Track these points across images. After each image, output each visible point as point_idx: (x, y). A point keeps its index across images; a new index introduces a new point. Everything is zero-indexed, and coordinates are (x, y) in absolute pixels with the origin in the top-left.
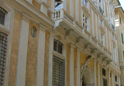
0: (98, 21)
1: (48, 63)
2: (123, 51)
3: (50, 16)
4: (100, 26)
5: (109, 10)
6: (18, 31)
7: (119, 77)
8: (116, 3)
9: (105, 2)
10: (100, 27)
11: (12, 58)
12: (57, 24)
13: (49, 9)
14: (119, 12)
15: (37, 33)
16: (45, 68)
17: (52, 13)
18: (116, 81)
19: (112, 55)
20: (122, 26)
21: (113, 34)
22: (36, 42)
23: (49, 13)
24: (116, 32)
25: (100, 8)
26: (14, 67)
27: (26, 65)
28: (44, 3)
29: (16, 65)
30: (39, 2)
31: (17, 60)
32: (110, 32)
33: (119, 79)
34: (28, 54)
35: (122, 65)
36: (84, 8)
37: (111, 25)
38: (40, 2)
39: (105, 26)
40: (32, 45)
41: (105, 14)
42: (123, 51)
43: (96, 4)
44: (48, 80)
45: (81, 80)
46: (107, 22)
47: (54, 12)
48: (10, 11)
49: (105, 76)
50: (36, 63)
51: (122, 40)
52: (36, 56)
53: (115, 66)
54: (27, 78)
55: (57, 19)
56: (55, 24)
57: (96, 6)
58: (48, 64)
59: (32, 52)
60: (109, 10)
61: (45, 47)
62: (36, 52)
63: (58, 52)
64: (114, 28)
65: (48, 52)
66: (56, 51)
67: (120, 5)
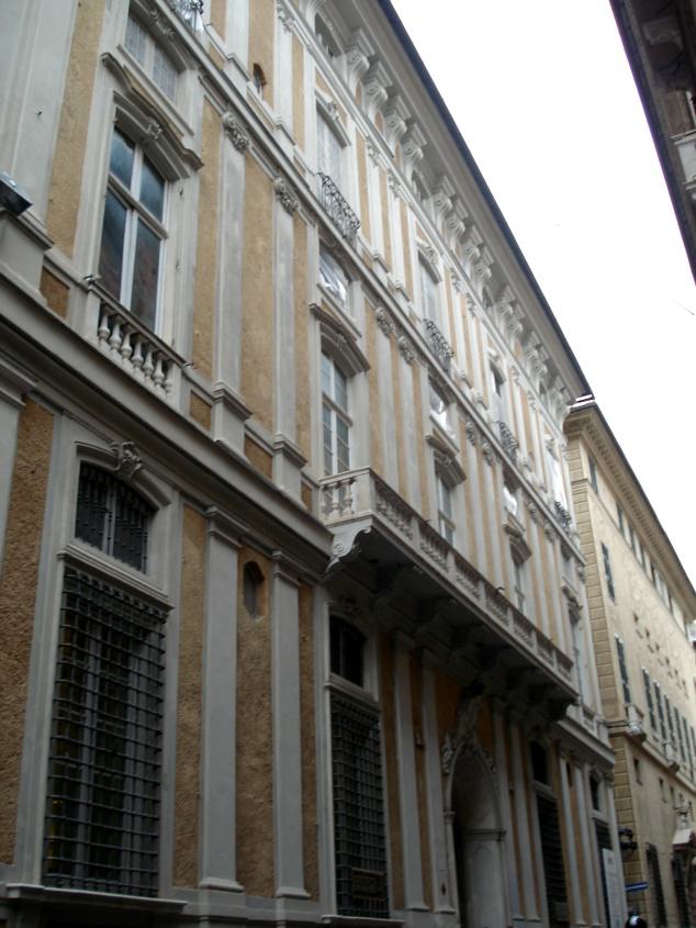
0: (497, 496)
1: (313, 738)
2: (110, 9)
3: (311, 499)
4: (435, 432)
5: (542, 428)
6: (196, 593)
7: (558, 756)
8: (568, 390)
9: (522, 391)
10: (432, 442)
11: (183, 727)
12: (343, 545)
13: (55, 253)
14: (584, 433)
15: (267, 593)
16: (304, 762)
17: (317, 487)
18: (596, 807)
19: (574, 669)
20: (600, 500)
21: (567, 552)
22: (266, 638)
23: (308, 487)
24: (578, 541)
25: (502, 426)
26: (189, 770)
27: (234, 756)
28: (286, 445)
29: (198, 761)
30: (264, 438)
31: (200, 735)
32: (554, 545)
33: (607, 798)
34: (239, 703)
35: (616, 715)
36: (438, 445)
37: (553, 508)
38: (271, 443)
39: (399, 353)
40: (252, 658)
41: (522, 456)
42: (110, 9)
43: (386, 271)
44: (317, 826)
45: (445, 810)
46: (536, 493)
47: (324, 483)
48: (166, 503)
49: (139, 568)
50: (269, 745)
51: (606, 577)
52: (269, 707)
53: (586, 723)
54: (239, 818)
55: (345, 518)
56: (336, 542)
57: (290, 155)
58: (314, 744)
59: (253, 693)
60: (538, 429)
61: (301, 657)
62: (267, 690)
63: (117, 555)
64: (514, 451)
65: (312, 682)
66: (100, 548)
67: (593, 398)
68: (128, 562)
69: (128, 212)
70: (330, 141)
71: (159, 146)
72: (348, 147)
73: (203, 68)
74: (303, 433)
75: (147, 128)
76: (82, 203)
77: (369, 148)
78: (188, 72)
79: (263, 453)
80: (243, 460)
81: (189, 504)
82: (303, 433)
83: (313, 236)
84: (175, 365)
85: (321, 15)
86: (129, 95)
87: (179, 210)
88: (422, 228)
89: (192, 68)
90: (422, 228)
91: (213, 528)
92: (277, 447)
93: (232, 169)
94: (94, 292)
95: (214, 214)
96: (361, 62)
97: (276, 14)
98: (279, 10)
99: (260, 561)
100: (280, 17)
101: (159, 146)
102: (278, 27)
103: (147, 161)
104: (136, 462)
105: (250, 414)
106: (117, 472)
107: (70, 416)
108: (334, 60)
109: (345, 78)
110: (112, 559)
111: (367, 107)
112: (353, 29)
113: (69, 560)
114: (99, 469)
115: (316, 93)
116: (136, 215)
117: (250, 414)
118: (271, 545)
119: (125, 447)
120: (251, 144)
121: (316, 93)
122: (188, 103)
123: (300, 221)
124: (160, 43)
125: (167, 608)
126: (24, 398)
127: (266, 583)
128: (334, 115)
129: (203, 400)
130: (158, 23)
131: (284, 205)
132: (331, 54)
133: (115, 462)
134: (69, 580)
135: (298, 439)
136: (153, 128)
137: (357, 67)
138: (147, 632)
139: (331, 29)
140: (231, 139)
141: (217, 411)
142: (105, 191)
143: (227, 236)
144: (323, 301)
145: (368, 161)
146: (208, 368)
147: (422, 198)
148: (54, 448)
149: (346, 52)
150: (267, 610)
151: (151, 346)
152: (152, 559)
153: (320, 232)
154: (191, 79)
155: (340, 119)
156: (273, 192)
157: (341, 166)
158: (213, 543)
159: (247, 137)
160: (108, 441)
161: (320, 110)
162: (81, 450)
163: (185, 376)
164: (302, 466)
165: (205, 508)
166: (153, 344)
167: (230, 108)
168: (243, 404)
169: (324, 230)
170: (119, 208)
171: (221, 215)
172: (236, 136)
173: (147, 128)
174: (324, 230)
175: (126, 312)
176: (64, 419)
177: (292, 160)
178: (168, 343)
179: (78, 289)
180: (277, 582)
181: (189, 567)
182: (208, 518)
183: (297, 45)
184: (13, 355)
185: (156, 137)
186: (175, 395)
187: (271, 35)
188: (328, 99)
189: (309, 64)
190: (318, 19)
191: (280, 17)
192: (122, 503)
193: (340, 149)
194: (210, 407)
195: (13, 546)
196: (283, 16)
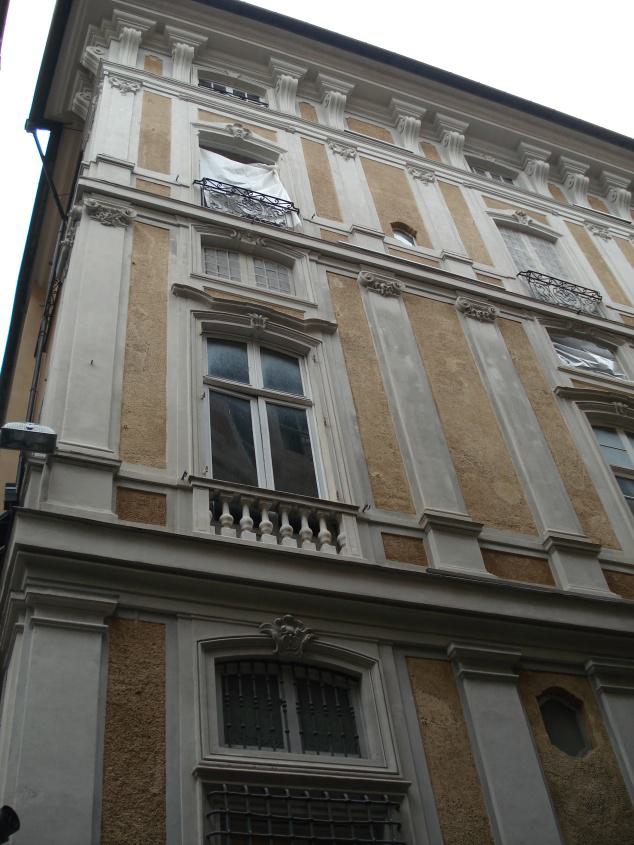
2: (175, 252)
6: (457, 761)
13: (605, 554)
15: (592, 718)
48: (368, 664)
68: (326, 751)
69: (253, 405)
70: (533, 245)
71: (268, 332)
72: (560, 240)
73: (312, 251)
74: (593, 520)
75: (249, 324)
76: (169, 414)
77: (591, 229)
78: (298, 263)
79: (528, 561)
80: (487, 579)
81: (410, 653)
82: (593, 520)
83: (536, 331)
84: (343, 516)
85: (467, 154)
86: (214, 307)
87: (321, 381)
88: (488, 195)
89: (300, 257)
90: (488, 195)
91: (599, 684)
92: (547, 548)
93: (385, 315)
94: (196, 486)
95: (372, 362)
96: (621, 195)
97: (590, 234)
98: (591, 229)
99: (566, 684)
100: (595, 234)
101: (268, 332)
102: (416, 186)
103: (265, 351)
104: (300, 635)
105: (599, 546)
106: (277, 653)
107: (187, 617)
108: (516, 184)
109: (531, 190)
110: (227, 751)
111: (573, 199)
112: (515, 148)
113: (209, 777)
114: (238, 661)
115: (490, 214)
116: (262, 402)
117: (599, 546)
118: (576, 658)
119: (279, 623)
120: (498, 311)
121: (490, 214)
122: (310, 287)
123: (140, 227)
124: (256, 255)
125: (402, 788)
126: (515, 670)
127: (587, 706)
128: (523, 222)
129: (411, 542)
130: (243, 240)
131: (476, 318)
132: (509, 180)
133: (270, 643)
134: (211, 796)
135: (586, 527)
136: (255, 320)
137: (620, 200)
138: (379, 829)
139: (493, 160)
140: (470, 317)
141: (430, 540)
142: (615, 480)
143: (395, 373)
144: (573, 380)
145: (597, 242)
146: (403, 503)
147: (509, 180)
148: (170, 658)
149: (523, 170)
150: (597, 736)
151: (301, 509)
152: (369, 737)
153: (542, 323)
154: (304, 267)
155: (535, 221)
156: (458, 313)
157: (560, 260)
158: (467, 686)
159: (393, 281)
160: (255, 625)
161: (501, 225)
162: (208, 647)
163: (361, 521)
164: (598, 553)
165: (443, 650)
166: (303, 506)
167: (459, 293)
168: (470, 520)
169: (546, 318)
170: (239, 405)
171: (382, 358)
172: (379, 286)
173: (249, 324)
174: (546, 318)
175: (270, 492)
176: (180, 624)
177: (475, 278)
178: (334, 499)
179: (179, 492)
180: (605, 700)
181: (434, 727)
182: (452, 661)
183: (450, 192)
184: (81, 582)
185: (264, 326)
186: (354, 544)
187: (409, 195)
188: (510, 212)
189: (474, 201)
190: (471, 162)
191: (595, 234)
192: (301, 687)
193: (551, 246)
194: (547, 560)
195: (119, 783)
196: (597, 231)
